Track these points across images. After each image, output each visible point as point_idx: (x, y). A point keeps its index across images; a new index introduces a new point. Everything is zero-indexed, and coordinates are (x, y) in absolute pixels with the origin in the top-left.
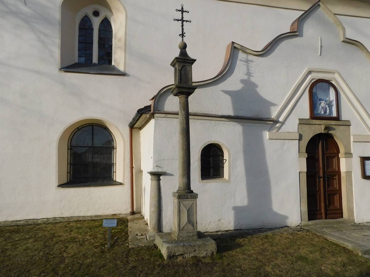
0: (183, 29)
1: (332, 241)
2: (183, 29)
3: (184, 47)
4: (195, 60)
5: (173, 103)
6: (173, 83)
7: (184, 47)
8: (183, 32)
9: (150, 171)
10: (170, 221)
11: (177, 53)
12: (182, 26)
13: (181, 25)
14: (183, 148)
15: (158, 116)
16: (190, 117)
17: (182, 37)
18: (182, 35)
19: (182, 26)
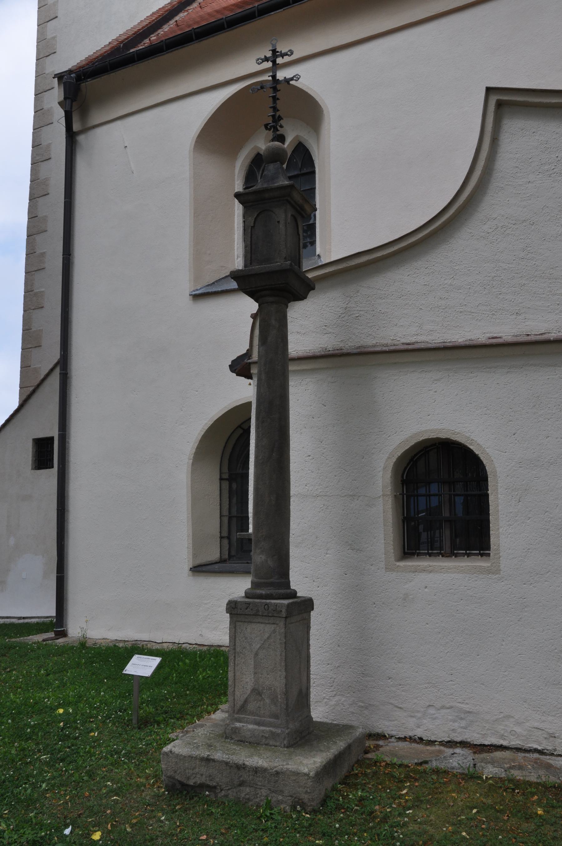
1: (495, 335)
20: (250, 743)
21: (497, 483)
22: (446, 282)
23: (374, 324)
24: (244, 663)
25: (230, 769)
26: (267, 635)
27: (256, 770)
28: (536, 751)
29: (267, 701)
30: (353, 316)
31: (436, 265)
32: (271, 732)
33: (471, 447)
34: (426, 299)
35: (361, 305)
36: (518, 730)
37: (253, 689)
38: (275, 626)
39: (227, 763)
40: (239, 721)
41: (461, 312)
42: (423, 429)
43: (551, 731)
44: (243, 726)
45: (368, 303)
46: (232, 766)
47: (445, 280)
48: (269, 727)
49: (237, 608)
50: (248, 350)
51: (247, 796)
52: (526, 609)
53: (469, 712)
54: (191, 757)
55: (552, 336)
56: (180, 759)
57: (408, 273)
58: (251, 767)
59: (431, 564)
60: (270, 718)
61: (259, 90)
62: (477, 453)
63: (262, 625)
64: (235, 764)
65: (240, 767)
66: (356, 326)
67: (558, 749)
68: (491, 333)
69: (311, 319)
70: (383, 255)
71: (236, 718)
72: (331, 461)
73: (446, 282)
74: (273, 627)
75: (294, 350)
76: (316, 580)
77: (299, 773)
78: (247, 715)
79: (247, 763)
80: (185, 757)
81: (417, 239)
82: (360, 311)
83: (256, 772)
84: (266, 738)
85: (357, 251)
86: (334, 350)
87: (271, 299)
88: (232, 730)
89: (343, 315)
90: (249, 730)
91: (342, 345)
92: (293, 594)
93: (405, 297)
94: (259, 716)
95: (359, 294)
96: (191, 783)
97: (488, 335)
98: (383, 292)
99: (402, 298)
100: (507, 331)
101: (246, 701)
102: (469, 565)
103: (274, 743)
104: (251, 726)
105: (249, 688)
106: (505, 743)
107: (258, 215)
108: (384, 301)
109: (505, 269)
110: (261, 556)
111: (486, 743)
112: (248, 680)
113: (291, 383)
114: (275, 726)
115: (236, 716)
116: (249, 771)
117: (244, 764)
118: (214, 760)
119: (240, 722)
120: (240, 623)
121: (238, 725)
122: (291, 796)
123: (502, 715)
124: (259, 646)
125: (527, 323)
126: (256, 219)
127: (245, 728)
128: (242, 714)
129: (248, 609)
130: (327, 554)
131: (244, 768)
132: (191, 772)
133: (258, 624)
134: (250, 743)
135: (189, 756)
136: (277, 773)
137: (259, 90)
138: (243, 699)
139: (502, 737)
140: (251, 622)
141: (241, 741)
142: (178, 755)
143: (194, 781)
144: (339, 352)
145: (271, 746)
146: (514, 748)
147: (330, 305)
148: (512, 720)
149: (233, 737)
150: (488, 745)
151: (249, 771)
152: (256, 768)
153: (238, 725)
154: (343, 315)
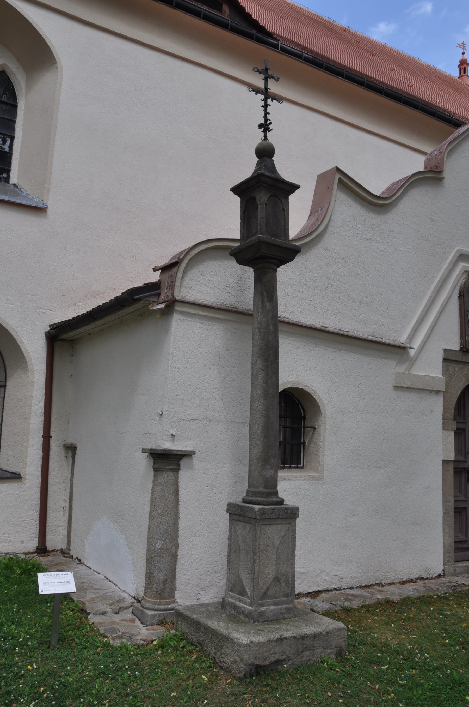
0: (266, 113)
1: (325, 325)
2: (266, 113)
3: (265, 153)
4: (298, 187)
5: (227, 282)
6: (239, 237)
7: (265, 153)
8: (266, 120)
9: (150, 447)
10: (200, 580)
11: (247, 168)
12: (266, 106)
13: (263, 103)
14: (267, 429)
15: (236, 519)
16: (279, 328)
17: (265, 131)
18: (265, 127)
19: (266, 106)
20: (272, 621)
21: (326, 422)
22: (303, 281)
24: (266, 558)
25: (297, 641)
26: (283, 533)
27: (315, 636)
28: (335, 589)
29: (283, 584)
32: (287, 608)
33: (315, 397)
36: (327, 578)
37: (275, 577)
38: (289, 525)
39: (295, 638)
40: (263, 605)
41: (309, 305)
42: (290, 380)
43: (341, 576)
44: (267, 609)
46: (298, 639)
48: (283, 605)
49: (264, 514)
51: (308, 658)
52: (334, 502)
53: (303, 573)
54: (269, 641)
55: (351, 334)
56: (260, 646)
58: (312, 635)
59: (288, 474)
60: (284, 597)
62: (317, 401)
63: (280, 526)
64: (300, 636)
65: (304, 637)
67: (343, 585)
68: (323, 323)
69: (216, 277)
71: (260, 604)
72: (231, 394)
73: (303, 281)
74: (287, 526)
75: (202, 298)
76: (214, 488)
77: (340, 629)
78: (267, 599)
79: (308, 633)
80: (264, 643)
83: (315, 637)
84: (283, 613)
86: (231, 307)
88: (259, 614)
89: (240, 282)
90: (271, 611)
91: (237, 305)
92: (281, 502)
94: (276, 598)
96: (267, 663)
97: (323, 325)
100: (331, 325)
101: (268, 589)
102: (305, 475)
103: (289, 616)
104: (272, 608)
105: (271, 577)
106: (320, 589)
109: (332, 285)
110: (271, 471)
111: (311, 591)
112: (270, 571)
113: (279, 338)
114: (287, 603)
115: (260, 602)
116: (310, 638)
117: (306, 634)
118: (286, 638)
119: (263, 606)
120: (264, 526)
121: (262, 609)
122: (336, 647)
123: (320, 571)
124: (279, 542)
125: (341, 323)
127: (268, 610)
128: (264, 600)
129: (273, 514)
130: (223, 467)
131: (307, 637)
132: (268, 654)
133: (277, 525)
134: (272, 621)
135: (268, 641)
136: (328, 633)
138: (265, 587)
139: (319, 585)
140: (272, 524)
141: (266, 621)
142: (258, 643)
143: (269, 661)
144: (234, 309)
145: (286, 619)
146: (325, 591)
147: (231, 271)
148: (325, 573)
149: (259, 619)
150: (312, 592)
151: (310, 638)
152: (315, 634)
153: (262, 609)
154: (240, 282)
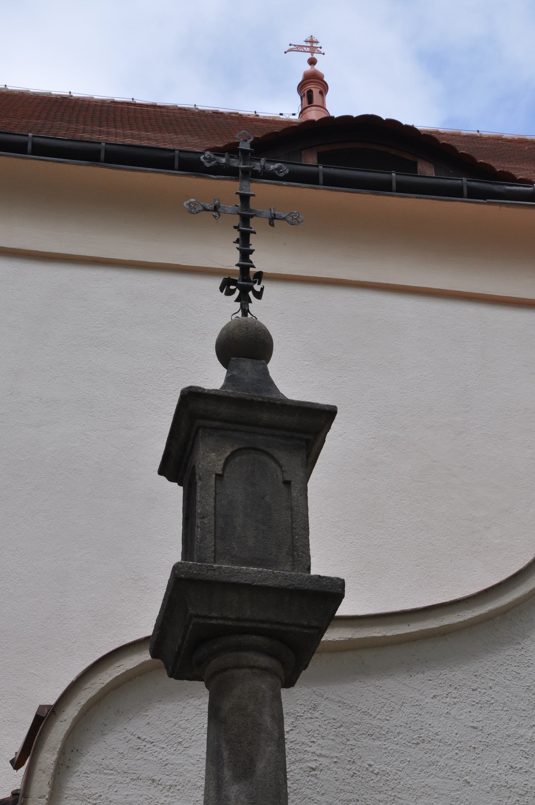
22: (521, 731)
23: (355, 796)
30: (304, 765)
31: (497, 688)
34: (479, 761)
35: (321, 742)
45: (339, 740)
47: (518, 726)
50: (15, 794)
57: (435, 692)
61: (205, 209)
66: (309, 792)
69: (190, 752)
70: (384, 637)
73: (521, 731)
81: (461, 619)
82: (320, 755)
85: (100, 655)
87: (264, 661)
93: (429, 746)
95: (317, 714)
98: (375, 722)
99: (423, 745)
107: (233, 454)
108: (378, 743)
126: (227, 460)
137: (205, 209)
